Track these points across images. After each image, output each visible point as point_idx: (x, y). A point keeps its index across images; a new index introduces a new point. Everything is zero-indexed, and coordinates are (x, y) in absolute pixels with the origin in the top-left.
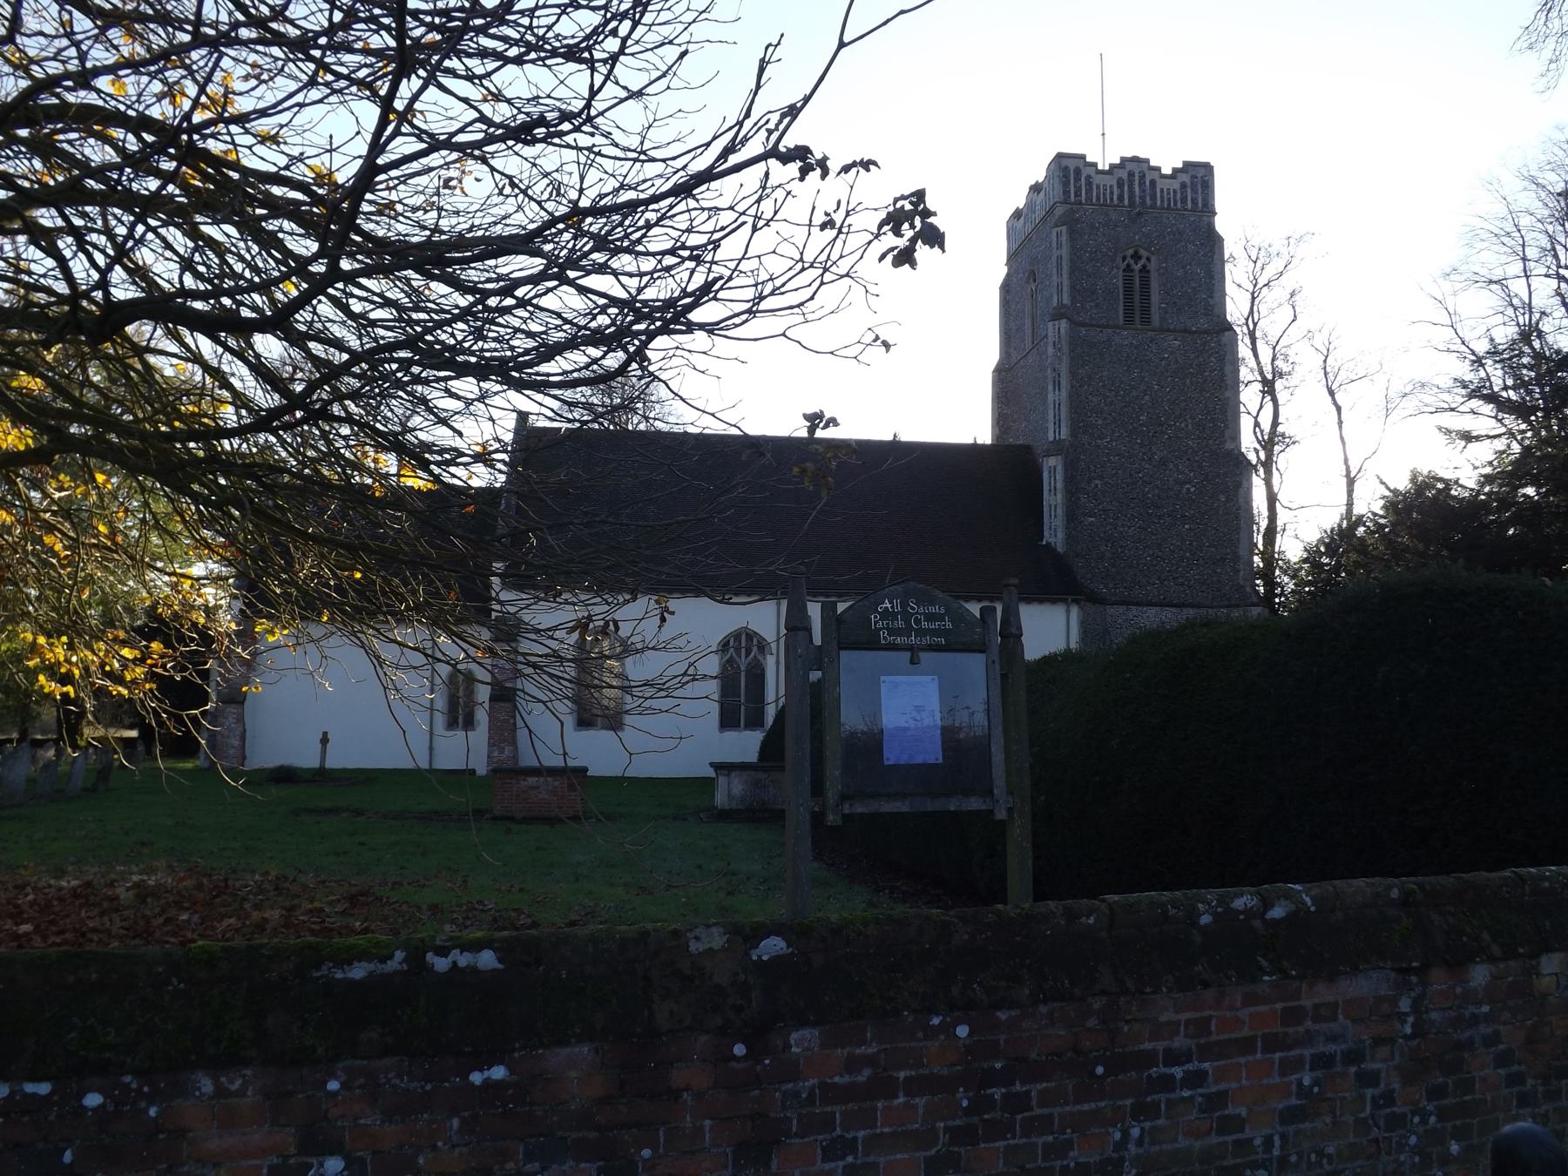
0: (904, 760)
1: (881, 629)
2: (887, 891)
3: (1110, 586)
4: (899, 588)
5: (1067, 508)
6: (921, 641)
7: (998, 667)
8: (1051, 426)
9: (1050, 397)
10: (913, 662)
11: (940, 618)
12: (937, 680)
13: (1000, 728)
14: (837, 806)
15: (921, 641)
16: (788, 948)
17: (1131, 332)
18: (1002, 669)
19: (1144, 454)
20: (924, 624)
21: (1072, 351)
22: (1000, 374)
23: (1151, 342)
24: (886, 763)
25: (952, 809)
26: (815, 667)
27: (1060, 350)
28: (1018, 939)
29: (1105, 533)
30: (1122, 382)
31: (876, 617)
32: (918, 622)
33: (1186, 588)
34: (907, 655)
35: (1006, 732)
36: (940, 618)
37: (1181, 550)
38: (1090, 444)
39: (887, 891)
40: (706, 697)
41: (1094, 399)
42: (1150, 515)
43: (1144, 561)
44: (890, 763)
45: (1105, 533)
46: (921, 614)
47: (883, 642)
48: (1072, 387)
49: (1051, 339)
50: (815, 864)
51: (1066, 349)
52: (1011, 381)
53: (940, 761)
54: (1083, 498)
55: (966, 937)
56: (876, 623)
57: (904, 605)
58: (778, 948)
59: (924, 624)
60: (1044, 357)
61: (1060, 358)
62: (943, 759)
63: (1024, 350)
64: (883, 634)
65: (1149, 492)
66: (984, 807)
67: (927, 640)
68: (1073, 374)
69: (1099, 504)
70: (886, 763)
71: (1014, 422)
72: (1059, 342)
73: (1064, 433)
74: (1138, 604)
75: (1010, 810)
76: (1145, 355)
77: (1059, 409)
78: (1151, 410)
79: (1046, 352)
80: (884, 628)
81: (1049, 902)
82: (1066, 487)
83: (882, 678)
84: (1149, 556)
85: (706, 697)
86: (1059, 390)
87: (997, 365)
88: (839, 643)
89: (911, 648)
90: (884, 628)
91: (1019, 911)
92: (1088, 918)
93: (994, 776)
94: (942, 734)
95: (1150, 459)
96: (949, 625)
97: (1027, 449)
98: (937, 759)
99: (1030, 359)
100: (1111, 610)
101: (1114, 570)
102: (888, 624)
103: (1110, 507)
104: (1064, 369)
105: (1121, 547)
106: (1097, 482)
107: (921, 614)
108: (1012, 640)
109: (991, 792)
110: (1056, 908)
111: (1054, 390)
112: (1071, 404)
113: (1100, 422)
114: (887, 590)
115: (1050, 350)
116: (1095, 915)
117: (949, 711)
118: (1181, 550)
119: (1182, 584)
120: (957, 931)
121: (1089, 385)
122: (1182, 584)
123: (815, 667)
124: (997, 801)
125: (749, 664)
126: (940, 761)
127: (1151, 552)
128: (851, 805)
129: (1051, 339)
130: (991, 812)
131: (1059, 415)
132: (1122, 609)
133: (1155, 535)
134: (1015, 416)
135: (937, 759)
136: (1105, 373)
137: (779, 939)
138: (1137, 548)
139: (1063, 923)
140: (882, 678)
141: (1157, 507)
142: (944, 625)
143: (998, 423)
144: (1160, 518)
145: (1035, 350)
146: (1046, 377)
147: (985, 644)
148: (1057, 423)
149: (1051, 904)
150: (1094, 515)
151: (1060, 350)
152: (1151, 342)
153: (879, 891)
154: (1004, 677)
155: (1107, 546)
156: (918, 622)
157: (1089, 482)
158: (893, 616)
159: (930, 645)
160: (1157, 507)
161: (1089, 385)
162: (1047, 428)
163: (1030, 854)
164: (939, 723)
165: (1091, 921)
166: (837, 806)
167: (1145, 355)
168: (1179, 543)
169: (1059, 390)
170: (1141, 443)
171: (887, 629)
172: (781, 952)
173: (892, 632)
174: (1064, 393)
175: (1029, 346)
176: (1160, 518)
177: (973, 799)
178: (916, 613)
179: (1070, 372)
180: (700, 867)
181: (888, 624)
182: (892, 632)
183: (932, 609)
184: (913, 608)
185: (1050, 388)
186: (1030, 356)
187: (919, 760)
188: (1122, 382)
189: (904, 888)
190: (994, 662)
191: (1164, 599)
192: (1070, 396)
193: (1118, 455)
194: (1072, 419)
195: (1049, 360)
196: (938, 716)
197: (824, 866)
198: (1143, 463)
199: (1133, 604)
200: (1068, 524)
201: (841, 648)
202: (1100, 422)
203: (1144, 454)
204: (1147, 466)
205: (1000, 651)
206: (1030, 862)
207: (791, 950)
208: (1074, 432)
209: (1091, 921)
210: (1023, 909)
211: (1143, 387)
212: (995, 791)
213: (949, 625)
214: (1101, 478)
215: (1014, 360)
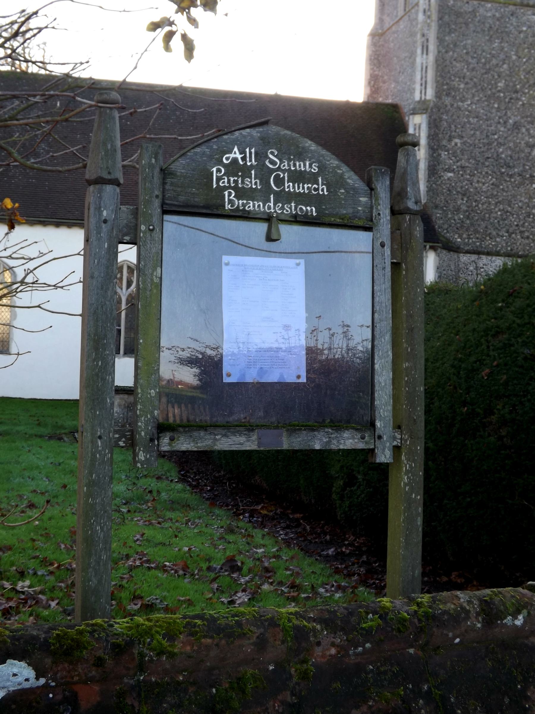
0: (251, 377)
1: (225, 188)
2: (247, 515)
3: (465, 236)
4: (255, 133)
5: (429, 162)
6: (282, 208)
7: (387, 251)
8: (418, 87)
9: (419, 60)
10: (269, 239)
11: (312, 178)
12: (302, 267)
13: (388, 337)
14: (152, 440)
15: (282, 208)
16: (37, 678)
17: (494, 5)
18: (393, 255)
19: (500, 118)
20: (289, 186)
21: (440, 19)
22: (373, 38)
23: (512, 15)
24: (226, 380)
25: (317, 447)
26: (127, 238)
27: (429, 17)
28: (412, 651)
29: (462, 187)
30: (484, 51)
31: (219, 171)
32: (279, 181)
33: (531, 241)
34: (263, 227)
35: (395, 344)
36: (312, 178)
37: (528, 206)
38: (452, 105)
39: (247, 515)
40: (39, 306)
41: (458, 65)
42: (503, 173)
43: (495, 215)
44: (232, 379)
45: (462, 187)
46: (284, 171)
47: (228, 207)
48: (439, 52)
49: (421, 8)
50: (180, 486)
51: (435, 17)
52: (383, 46)
53: (303, 380)
54: (444, 154)
55: (333, 651)
56: (219, 179)
57: (261, 156)
58: (20, 679)
59: (289, 186)
60: (414, 23)
61: (429, 25)
62: (308, 378)
63: (397, 16)
64: (229, 196)
65: (502, 153)
66: (361, 446)
67: (291, 208)
68: (440, 40)
69: (458, 162)
70: (226, 380)
71: (384, 82)
72: (429, 10)
73: (430, 94)
74: (488, 254)
75: (397, 450)
76: (506, 27)
77: (426, 71)
78: (508, 78)
79: (416, 19)
80: (230, 187)
81: (458, 593)
82: (429, 144)
83: (225, 259)
84: (500, 210)
85: (39, 306)
86: (427, 54)
87: (372, 30)
88: (163, 204)
89: (268, 219)
90: (230, 187)
91: (415, 608)
92: (515, 618)
93: (377, 403)
94: (307, 354)
95: (505, 123)
96: (323, 190)
97: (395, 107)
98: (299, 377)
99: (402, 25)
100: (464, 258)
101: (468, 222)
102: (236, 182)
103: (467, 164)
104: (432, 36)
105: (476, 201)
106: (457, 140)
107: (284, 171)
108: (408, 217)
109: (373, 425)
110: (469, 602)
111: (423, 53)
112: (437, 68)
113: (462, 86)
114: (237, 133)
115: (421, 17)
116: (525, 612)
117: (313, 332)
118: (528, 206)
119: (528, 238)
120: (319, 644)
121: (454, 52)
122: (528, 238)
123: (127, 238)
124: (380, 437)
125: (130, 295)
126: (303, 380)
127: (501, 207)
128: (172, 439)
129: (421, 8)
130: (372, 452)
131: (426, 77)
132: (474, 257)
133: (507, 192)
134: (386, 78)
135: (299, 377)
136: (469, 42)
137: (23, 664)
138: (490, 203)
139: (479, 625)
140: (225, 259)
141: (509, 167)
142: (316, 190)
143: (369, 83)
144: (511, 176)
145: (406, 18)
146: (415, 42)
147: (372, 220)
148: (424, 85)
149: (463, 596)
150: (453, 171)
151: (429, 17)
152: (512, 15)
153: (240, 514)
154: (395, 266)
155: (462, 199)
156: (279, 181)
157: (450, 140)
158: (245, 171)
159: (296, 216)
160: (509, 167)
161: (454, 52)
162: (414, 89)
163: (420, 510)
164: (303, 342)
165: (519, 621)
166: (152, 440)
167: (506, 27)
168: (527, 200)
169: (427, 54)
170: (498, 108)
171: (236, 188)
172: (27, 685)
173: (241, 193)
174: (431, 57)
175: (401, 13)
176: (511, 176)
177: (346, 434)
178: (279, 169)
179: (438, 38)
180: (65, 486)
181: (236, 182)
182: (241, 193)
183: (300, 166)
184: (273, 162)
185: (419, 51)
186: (401, 22)
187: (273, 377)
188: (484, 51)
189: (264, 512)
190: (383, 245)
191: (511, 250)
192: (437, 61)
193: (477, 117)
194: (437, 82)
195: (419, 26)
196: (303, 337)
197: (188, 488)
198: (499, 126)
199: (483, 253)
200: (429, 177)
201: (165, 212)
202: (462, 86)
203: (500, 118)
204: (502, 129)
205: (392, 233)
206: (419, 521)
207: (42, 681)
208: (438, 95)
209: (519, 621)
210: (419, 605)
211: (502, 56)
212: (378, 424)
213: (323, 190)
214: (461, 137)
215: (387, 26)
